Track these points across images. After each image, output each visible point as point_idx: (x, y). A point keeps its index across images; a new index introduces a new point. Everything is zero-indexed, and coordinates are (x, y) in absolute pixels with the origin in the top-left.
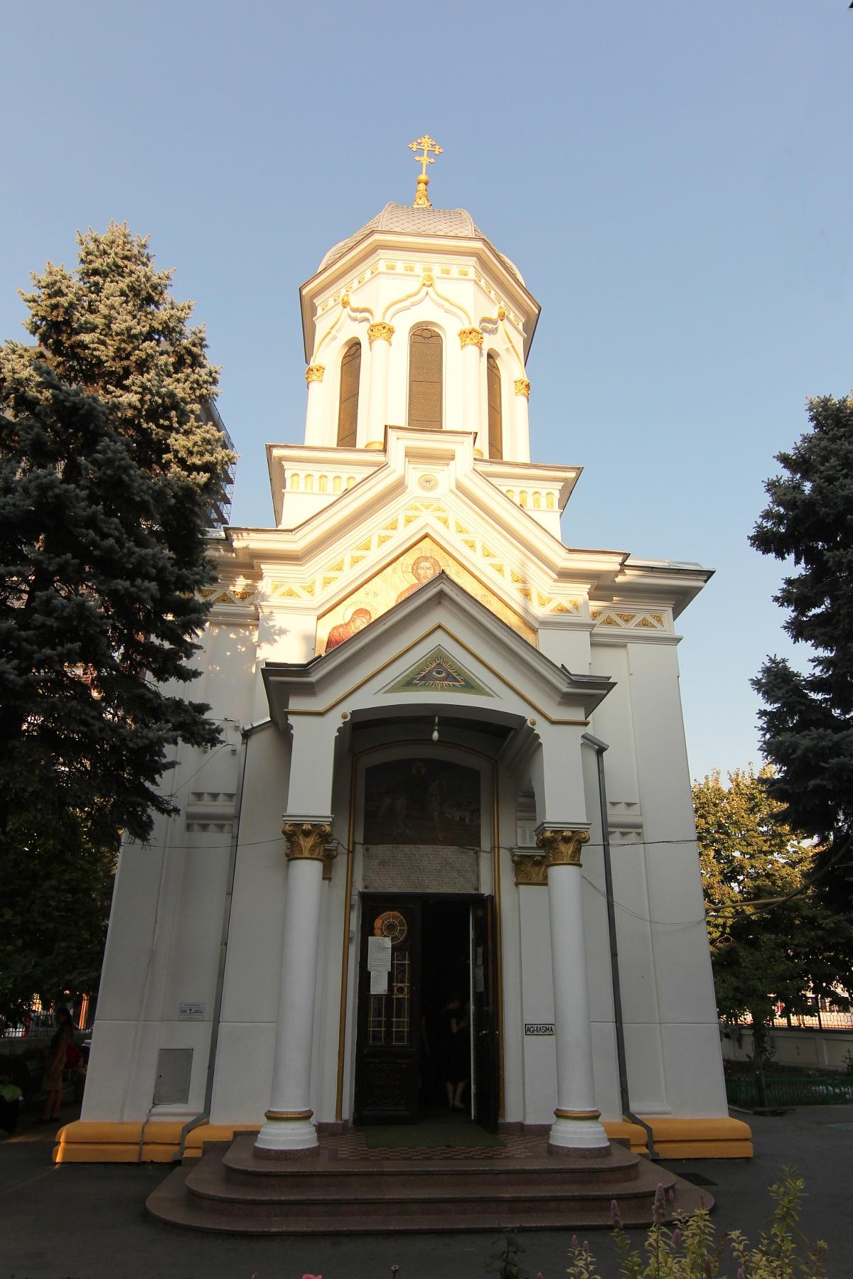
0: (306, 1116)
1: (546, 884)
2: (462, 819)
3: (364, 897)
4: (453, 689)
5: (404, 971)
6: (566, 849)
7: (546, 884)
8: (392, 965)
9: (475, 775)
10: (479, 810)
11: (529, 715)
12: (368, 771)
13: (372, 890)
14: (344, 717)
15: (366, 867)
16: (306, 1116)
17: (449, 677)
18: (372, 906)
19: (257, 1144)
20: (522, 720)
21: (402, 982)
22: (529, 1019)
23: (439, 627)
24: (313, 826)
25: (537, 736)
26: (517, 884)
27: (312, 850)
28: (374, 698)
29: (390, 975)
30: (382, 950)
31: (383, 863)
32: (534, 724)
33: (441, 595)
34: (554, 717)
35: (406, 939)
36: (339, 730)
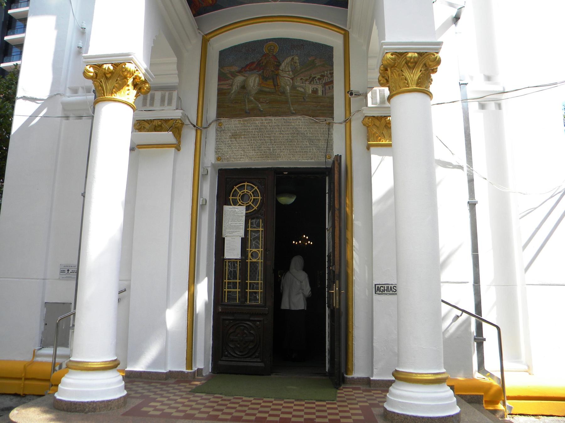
0: (113, 366)
2: (315, 91)
6: (414, 76)
8: (246, 232)
10: (332, 82)
12: (223, 53)
15: (218, 141)
16: (113, 366)
18: (230, 183)
19: (58, 396)
21: (257, 247)
22: (379, 280)
29: (244, 241)
30: (236, 216)
31: (235, 136)
35: (260, 208)
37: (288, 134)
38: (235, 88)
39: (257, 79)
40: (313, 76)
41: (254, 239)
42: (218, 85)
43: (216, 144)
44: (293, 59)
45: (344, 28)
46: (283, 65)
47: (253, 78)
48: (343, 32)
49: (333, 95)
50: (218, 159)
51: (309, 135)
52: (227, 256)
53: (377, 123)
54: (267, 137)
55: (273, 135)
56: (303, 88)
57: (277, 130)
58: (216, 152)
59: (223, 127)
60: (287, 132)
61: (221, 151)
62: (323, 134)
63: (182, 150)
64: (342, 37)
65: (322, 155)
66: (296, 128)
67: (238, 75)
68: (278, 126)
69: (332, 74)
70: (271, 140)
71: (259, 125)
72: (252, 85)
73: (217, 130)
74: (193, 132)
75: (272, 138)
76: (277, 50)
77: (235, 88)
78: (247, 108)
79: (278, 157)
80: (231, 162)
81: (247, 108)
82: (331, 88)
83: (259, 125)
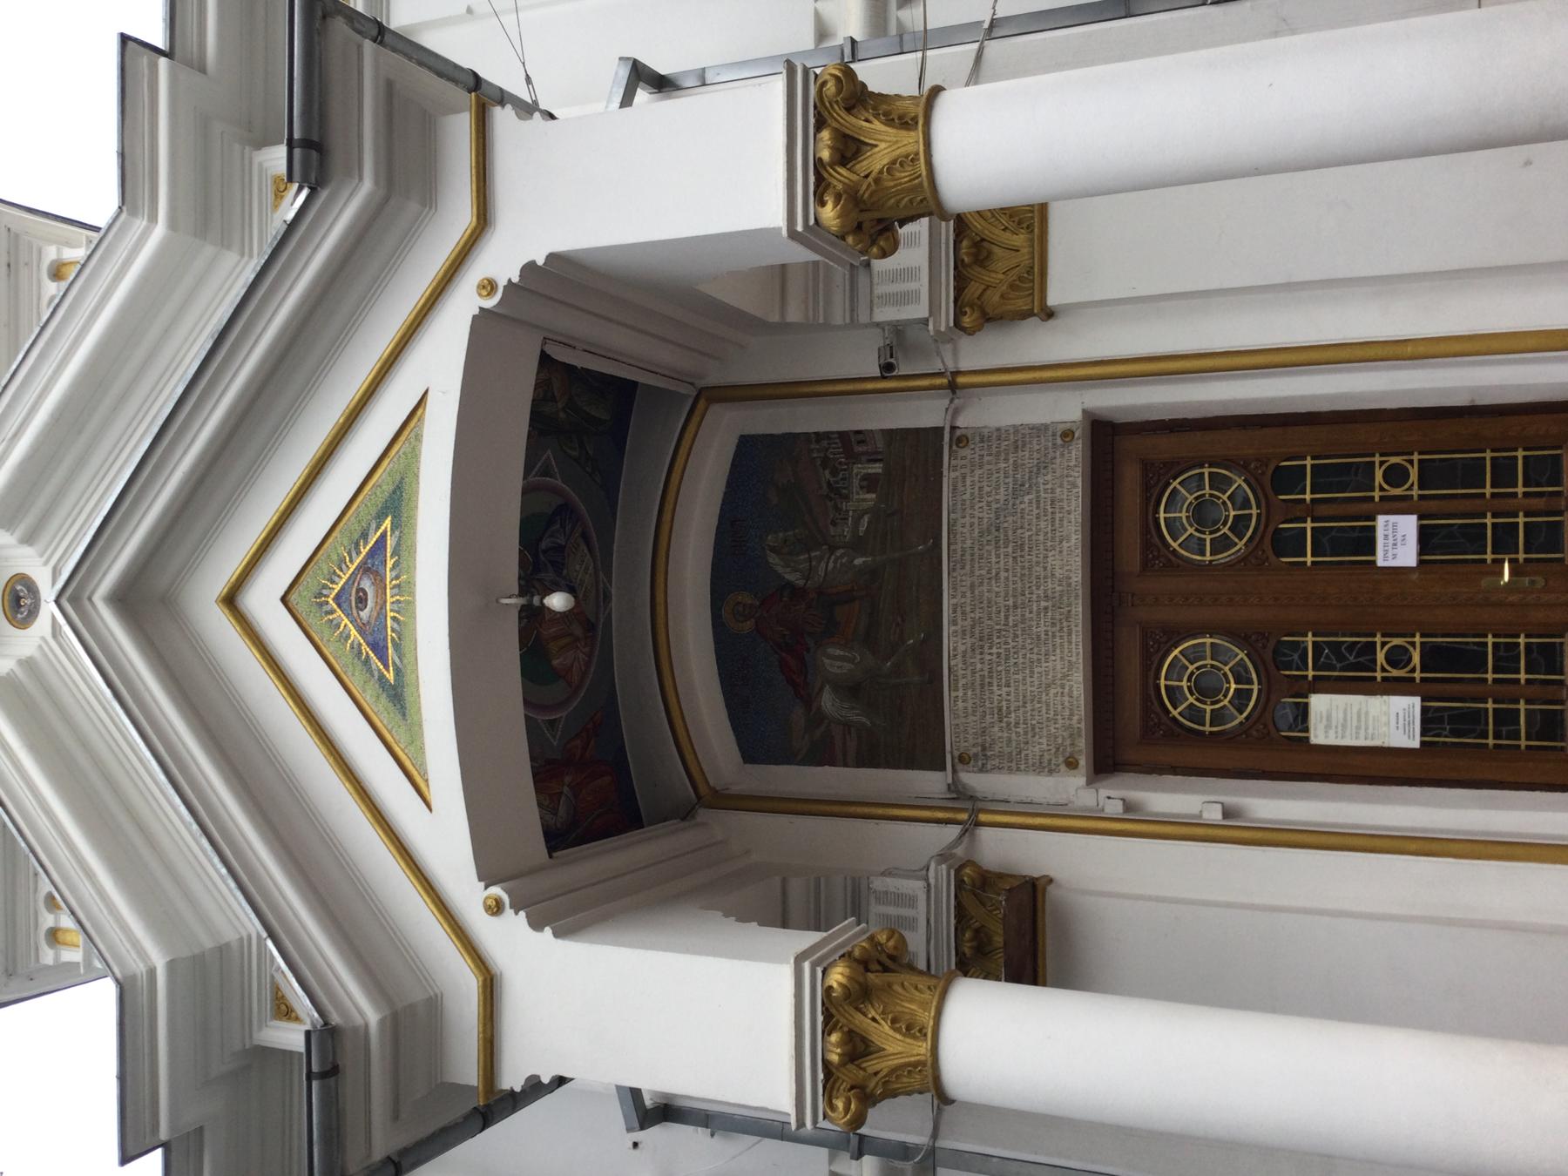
1: (1042, 210)
2: (870, 483)
3: (1108, 760)
4: (405, 550)
5: (1335, 647)
6: (885, 145)
7: (1042, 210)
9: (753, 456)
10: (843, 436)
11: (463, 305)
12: (754, 750)
13: (1083, 744)
14: (496, 908)
15: (1014, 762)
17: (372, 567)
20: (483, 321)
23: (231, 600)
24: (830, 1024)
25: (529, 268)
26: (1049, 314)
27: (912, 1030)
28: (444, 834)
32: (488, 286)
33: (127, 600)
34: (458, 214)
36: (536, 924)
37: (998, 556)
38: (856, 716)
39: (830, 650)
40: (825, 490)
41: (1341, 658)
42: (846, 765)
43: (1026, 771)
44: (773, 550)
45: (690, 401)
46: (791, 577)
47: (827, 661)
48: (702, 404)
49: (882, 430)
50: (1072, 764)
51: (1001, 497)
52: (1410, 739)
53: (973, 290)
54: (1007, 618)
55: (1000, 600)
56: (861, 517)
57: (985, 588)
58: (1051, 772)
59: (974, 750)
60: (994, 560)
61: (1047, 757)
62: (998, 454)
63: (1052, 874)
64: (716, 408)
65: (1062, 455)
66: (981, 534)
67: (819, 707)
68: (972, 586)
69: (819, 436)
70: (1015, 607)
71: (969, 641)
72: (848, 666)
73: (982, 770)
74: (985, 834)
75: (1010, 603)
76: (746, 598)
77: (856, 716)
78: (916, 678)
79: (1069, 585)
80: (1082, 726)
81: (916, 678)
82: (860, 437)
83: (969, 641)
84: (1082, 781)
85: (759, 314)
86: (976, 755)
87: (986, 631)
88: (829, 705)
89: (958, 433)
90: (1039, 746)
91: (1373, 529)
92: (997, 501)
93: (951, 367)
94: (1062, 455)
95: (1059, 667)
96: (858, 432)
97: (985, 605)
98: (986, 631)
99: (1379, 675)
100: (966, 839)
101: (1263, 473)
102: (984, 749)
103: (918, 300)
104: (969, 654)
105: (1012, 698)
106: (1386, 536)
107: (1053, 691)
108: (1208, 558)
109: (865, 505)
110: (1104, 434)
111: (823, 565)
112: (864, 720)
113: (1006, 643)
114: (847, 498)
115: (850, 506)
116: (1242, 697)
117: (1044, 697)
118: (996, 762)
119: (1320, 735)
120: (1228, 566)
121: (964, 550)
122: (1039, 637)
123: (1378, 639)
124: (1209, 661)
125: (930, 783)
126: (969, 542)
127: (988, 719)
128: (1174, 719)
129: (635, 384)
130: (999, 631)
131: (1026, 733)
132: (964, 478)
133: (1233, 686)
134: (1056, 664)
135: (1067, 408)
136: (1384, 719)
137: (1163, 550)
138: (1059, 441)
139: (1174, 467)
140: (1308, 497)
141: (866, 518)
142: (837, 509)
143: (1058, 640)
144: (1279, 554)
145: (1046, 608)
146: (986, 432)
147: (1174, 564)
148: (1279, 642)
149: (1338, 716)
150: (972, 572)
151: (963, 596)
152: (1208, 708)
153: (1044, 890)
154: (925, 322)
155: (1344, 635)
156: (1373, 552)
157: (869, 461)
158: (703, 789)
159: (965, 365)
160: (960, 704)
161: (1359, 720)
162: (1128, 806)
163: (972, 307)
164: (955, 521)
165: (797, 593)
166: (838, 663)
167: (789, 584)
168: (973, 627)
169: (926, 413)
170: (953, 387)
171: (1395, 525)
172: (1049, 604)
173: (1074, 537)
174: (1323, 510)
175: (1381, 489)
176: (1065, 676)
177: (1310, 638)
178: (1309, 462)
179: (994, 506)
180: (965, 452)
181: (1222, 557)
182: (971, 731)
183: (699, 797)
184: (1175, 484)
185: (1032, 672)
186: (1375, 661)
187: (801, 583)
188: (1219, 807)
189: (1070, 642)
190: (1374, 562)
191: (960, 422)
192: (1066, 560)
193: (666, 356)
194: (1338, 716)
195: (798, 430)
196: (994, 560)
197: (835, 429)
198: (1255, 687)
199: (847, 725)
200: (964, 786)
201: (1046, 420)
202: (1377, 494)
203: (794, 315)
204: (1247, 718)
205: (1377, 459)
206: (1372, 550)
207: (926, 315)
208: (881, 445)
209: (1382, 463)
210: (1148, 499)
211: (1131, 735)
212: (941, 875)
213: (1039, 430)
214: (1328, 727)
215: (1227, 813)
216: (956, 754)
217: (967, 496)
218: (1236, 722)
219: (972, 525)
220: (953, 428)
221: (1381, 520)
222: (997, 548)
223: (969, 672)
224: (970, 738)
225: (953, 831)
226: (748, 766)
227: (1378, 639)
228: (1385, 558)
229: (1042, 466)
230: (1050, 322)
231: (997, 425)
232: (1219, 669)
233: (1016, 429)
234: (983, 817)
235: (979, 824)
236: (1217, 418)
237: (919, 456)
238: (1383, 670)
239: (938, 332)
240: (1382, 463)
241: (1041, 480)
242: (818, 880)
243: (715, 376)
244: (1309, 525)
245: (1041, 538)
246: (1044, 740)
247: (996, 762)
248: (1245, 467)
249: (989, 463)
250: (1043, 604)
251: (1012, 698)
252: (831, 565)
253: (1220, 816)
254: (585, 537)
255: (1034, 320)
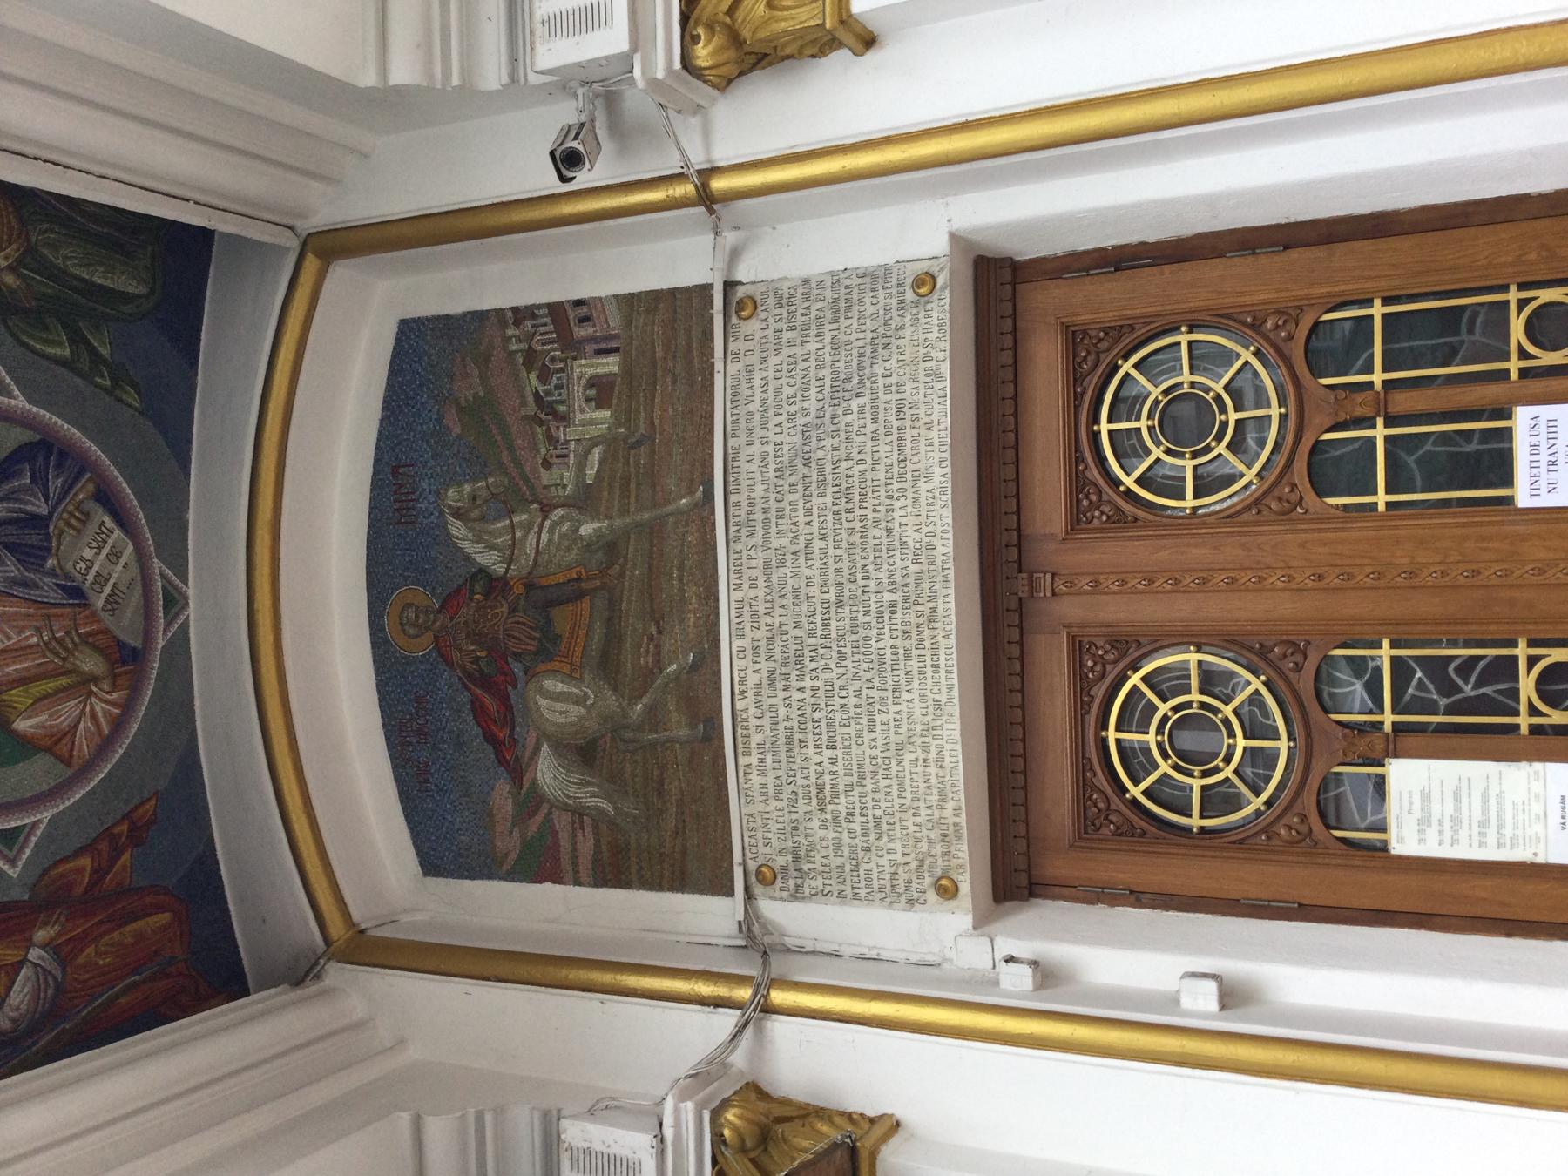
2: (601, 391)
3: (1016, 876)
5: (1435, 667)
10: (556, 310)
12: (440, 855)
15: (849, 885)
37: (808, 512)
38: (593, 799)
39: (548, 684)
41: (1449, 688)
43: (868, 899)
44: (457, 513)
46: (489, 560)
47: (543, 702)
50: (947, 891)
51: (812, 404)
54: (826, 623)
56: (588, 452)
57: (788, 571)
59: (780, 861)
60: (802, 519)
61: (903, 876)
62: (806, 327)
63: (899, 1112)
64: (342, 274)
67: (534, 780)
68: (767, 568)
69: (521, 314)
72: (576, 711)
73: (796, 895)
74: (780, 1026)
75: (832, 596)
76: (419, 595)
77: (593, 799)
80: (963, 820)
82: (584, 310)
83: (765, 666)
84: (965, 920)
85: (335, 71)
86: (784, 869)
87: (792, 648)
88: (548, 777)
89: (741, 292)
90: (889, 857)
91: (1507, 434)
92: (806, 412)
93: (698, 160)
94: (915, 320)
95: (917, 712)
96: (579, 303)
97: (789, 601)
98: (792, 648)
99: (1524, 721)
100: (749, 1032)
101: (1290, 337)
102: (797, 859)
103: (609, 20)
104: (766, 690)
105: (839, 768)
106: (1535, 447)
107: (909, 757)
108: (1190, 502)
109: (593, 431)
110: (998, 284)
111: (532, 538)
112: (603, 804)
113: (827, 669)
114: (564, 419)
115: (571, 433)
116: (1260, 760)
117: (894, 768)
118: (818, 883)
119: (1409, 837)
120: (1229, 517)
121: (751, 503)
122: (881, 658)
123: (1522, 651)
124: (1195, 697)
125: (710, 917)
126: (759, 488)
127: (802, 806)
128: (1134, 801)
129: (212, 233)
130: (814, 648)
131: (865, 833)
132: (750, 373)
133: (1241, 743)
134: (911, 706)
135: (920, 230)
136: (1537, 808)
137: (1108, 491)
138: (910, 296)
139: (1126, 335)
140: (1377, 377)
141: (596, 454)
142: (551, 439)
143: (914, 663)
144: (1320, 493)
145: (893, 605)
146: (785, 288)
147: (1128, 517)
148: (1326, 658)
149: (1442, 808)
150: (766, 542)
151: (753, 586)
152: (1197, 784)
153: (873, 1156)
154: (626, 60)
155: (1453, 643)
156: (1507, 479)
157: (599, 353)
158: (337, 929)
159: (722, 156)
160: (755, 779)
161: (1485, 810)
162: (1046, 975)
163: (710, 27)
164: (737, 450)
165: (494, 585)
166: (559, 706)
167: (483, 570)
168: (771, 639)
169: (677, 259)
170: (706, 198)
171: (1552, 425)
172: (898, 597)
173: (938, 471)
174: (1403, 402)
175: (1523, 354)
176: (929, 729)
177: (1386, 652)
178: (1377, 310)
179: (801, 421)
180: (753, 326)
181: (1215, 501)
182: (774, 827)
183: (328, 941)
184: (1127, 367)
185: (872, 722)
186: (1514, 694)
187: (500, 569)
188: (1211, 987)
189: (935, 667)
190: (1509, 500)
191: (742, 274)
192: (930, 515)
193: (250, 182)
194: (1442, 808)
195: (486, 307)
196: (802, 519)
197: (544, 300)
198: (1283, 745)
199: (578, 812)
200: (766, 926)
201: (888, 258)
202: (1514, 365)
203: (403, 72)
204: (1269, 803)
205: (1513, 295)
206: (1506, 477)
207: (624, 46)
208: (615, 321)
209: (1522, 304)
210: (1078, 398)
211: (1054, 829)
212: (685, 1121)
213: (875, 277)
214: (1424, 822)
215: (1231, 996)
216: (752, 866)
217: (755, 406)
218: (1248, 811)
219: (764, 456)
220: (729, 286)
221: (1523, 416)
222: (807, 497)
223: (766, 722)
224: (774, 842)
225: (728, 1019)
226: (431, 881)
227: (1522, 651)
228: (1534, 491)
229: (879, 345)
230: (872, 56)
231: (805, 272)
232: (1215, 711)
233: (836, 279)
234: (778, 997)
235: (769, 1010)
236: (1200, 236)
237: (673, 337)
238: (1533, 711)
239: (653, 83)
240: (1522, 304)
241: (878, 369)
242: (480, 1117)
243: (330, 210)
244: (1380, 432)
245: (881, 475)
246: (897, 846)
247: (818, 883)
248: (1256, 326)
249: (791, 344)
250: (888, 597)
251: (839, 768)
252: (545, 537)
253: (1213, 1005)
254: (106, 498)
255: (843, 55)
